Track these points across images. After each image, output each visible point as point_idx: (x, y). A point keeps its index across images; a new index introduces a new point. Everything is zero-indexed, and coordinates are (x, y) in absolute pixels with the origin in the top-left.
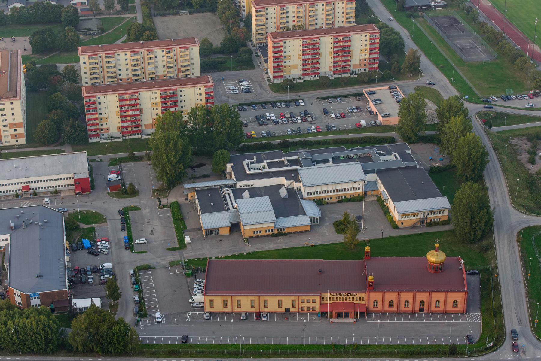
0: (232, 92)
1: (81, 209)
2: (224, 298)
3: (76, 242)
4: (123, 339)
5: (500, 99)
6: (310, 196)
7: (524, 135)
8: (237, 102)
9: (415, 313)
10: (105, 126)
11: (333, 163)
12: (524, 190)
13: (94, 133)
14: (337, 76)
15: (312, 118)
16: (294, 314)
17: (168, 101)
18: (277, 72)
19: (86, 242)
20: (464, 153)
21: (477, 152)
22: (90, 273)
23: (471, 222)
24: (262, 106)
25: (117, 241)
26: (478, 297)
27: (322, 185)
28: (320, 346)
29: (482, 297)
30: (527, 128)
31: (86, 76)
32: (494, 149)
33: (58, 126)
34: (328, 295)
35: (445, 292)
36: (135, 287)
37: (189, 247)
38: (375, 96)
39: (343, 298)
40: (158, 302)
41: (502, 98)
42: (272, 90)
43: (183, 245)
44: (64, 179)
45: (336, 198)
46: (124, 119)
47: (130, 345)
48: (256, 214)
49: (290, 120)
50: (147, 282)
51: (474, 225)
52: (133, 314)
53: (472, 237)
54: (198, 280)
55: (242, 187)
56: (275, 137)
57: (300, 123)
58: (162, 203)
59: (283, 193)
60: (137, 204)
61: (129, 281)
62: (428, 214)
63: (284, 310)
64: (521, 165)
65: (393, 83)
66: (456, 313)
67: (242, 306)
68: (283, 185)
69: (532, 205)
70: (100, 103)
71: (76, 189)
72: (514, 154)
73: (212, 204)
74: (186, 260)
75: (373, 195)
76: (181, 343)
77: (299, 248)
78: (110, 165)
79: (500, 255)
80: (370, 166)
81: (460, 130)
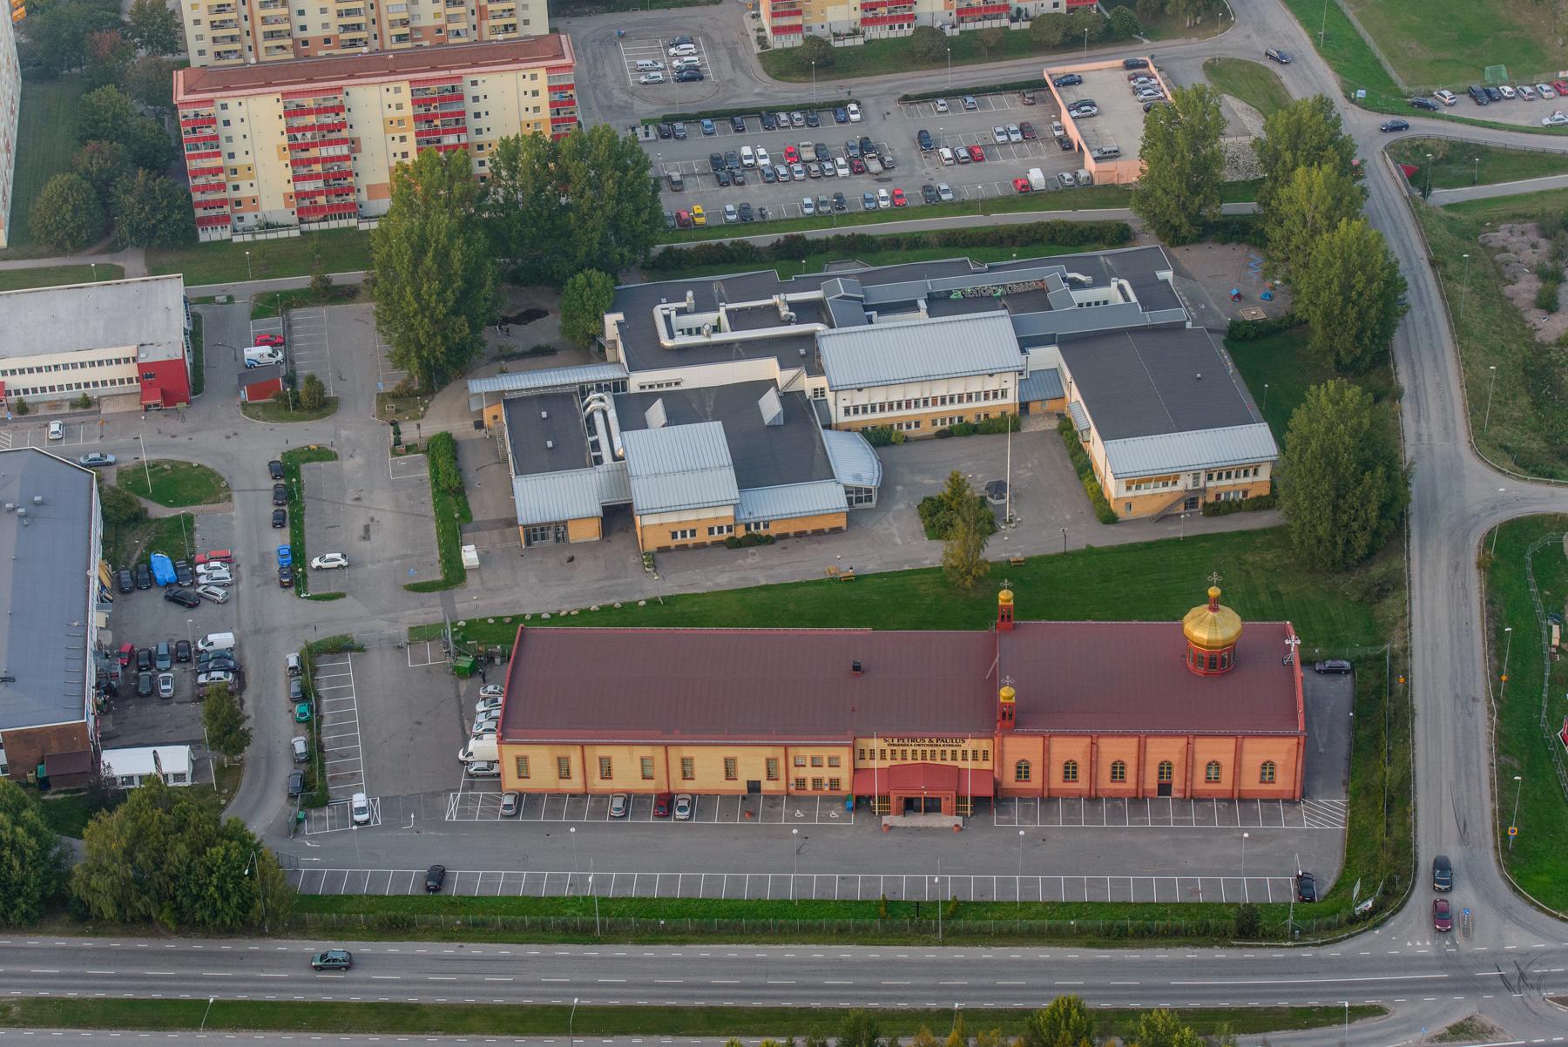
0: (643, 79)
1: (156, 457)
2: (561, 751)
3: (133, 563)
4: (237, 884)
5: (1466, 97)
6: (853, 418)
7: (1531, 217)
8: (657, 110)
9: (1144, 798)
10: (245, 192)
11: (930, 313)
12: (1514, 396)
13: (213, 212)
14: (970, 26)
15: (882, 162)
16: (773, 799)
17: (436, 116)
18: (784, 14)
19: (163, 566)
20: (1329, 283)
21: (1370, 281)
22: (167, 664)
23: (1336, 508)
24: (733, 122)
25: (256, 561)
26: (1342, 745)
27: (887, 384)
28: (848, 905)
29: (1356, 748)
30: (1542, 194)
31: (199, 30)
32: (1433, 264)
33: (103, 188)
34: (876, 744)
35: (1235, 736)
36: (299, 709)
37: (472, 581)
38: (1081, 92)
39: (924, 753)
40: (366, 758)
41: (1473, 94)
42: (767, 70)
43: (455, 574)
44: (110, 362)
45: (934, 423)
46: (303, 171)
47: (259, 904)
48: (680, 475)
49: (815, 167)
50: (335, 693)
51: (1345, 517)
52: (285, 797)
53: (1339, 554)
54: (490, 688)
55: (647, 390)
56: (766, 225)
57: (844, 177)
58: (403, 438)
59: (770, 407)
60: (325, 441)
61: (284, 688)
62: (1210, 477)
63: (745, 788)
64: (1512, 314)
65: (1138, 47)
66: (1271, 800)
67: (615, 773)
68: (773, 382)
69: (1537, 445)
70: (227, 123)
71: (143, 396)
72: (1492, 278)
73: (550, 444)
74: (462, 623)
75: (1048, 414)
76: (422, 892)
77: (807, 583)
78: (255, 315)
79: (1422, 612)
80: (1040, 322)
81: (1322, 208)
